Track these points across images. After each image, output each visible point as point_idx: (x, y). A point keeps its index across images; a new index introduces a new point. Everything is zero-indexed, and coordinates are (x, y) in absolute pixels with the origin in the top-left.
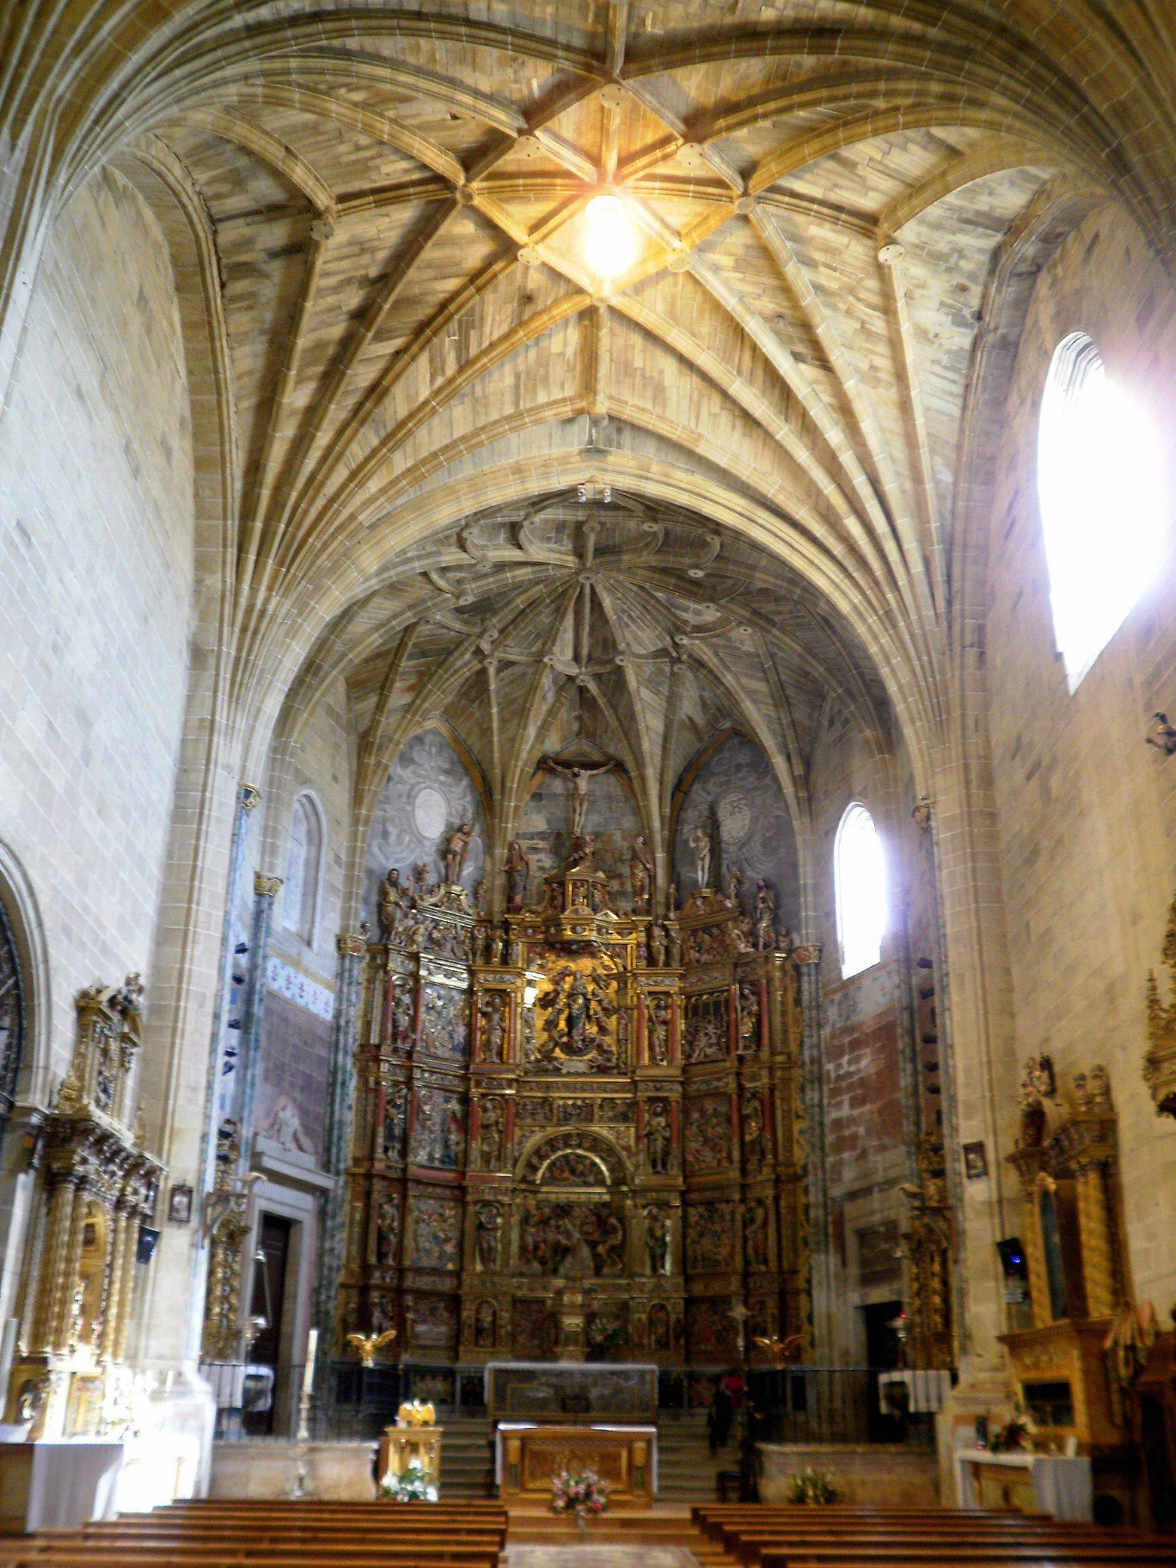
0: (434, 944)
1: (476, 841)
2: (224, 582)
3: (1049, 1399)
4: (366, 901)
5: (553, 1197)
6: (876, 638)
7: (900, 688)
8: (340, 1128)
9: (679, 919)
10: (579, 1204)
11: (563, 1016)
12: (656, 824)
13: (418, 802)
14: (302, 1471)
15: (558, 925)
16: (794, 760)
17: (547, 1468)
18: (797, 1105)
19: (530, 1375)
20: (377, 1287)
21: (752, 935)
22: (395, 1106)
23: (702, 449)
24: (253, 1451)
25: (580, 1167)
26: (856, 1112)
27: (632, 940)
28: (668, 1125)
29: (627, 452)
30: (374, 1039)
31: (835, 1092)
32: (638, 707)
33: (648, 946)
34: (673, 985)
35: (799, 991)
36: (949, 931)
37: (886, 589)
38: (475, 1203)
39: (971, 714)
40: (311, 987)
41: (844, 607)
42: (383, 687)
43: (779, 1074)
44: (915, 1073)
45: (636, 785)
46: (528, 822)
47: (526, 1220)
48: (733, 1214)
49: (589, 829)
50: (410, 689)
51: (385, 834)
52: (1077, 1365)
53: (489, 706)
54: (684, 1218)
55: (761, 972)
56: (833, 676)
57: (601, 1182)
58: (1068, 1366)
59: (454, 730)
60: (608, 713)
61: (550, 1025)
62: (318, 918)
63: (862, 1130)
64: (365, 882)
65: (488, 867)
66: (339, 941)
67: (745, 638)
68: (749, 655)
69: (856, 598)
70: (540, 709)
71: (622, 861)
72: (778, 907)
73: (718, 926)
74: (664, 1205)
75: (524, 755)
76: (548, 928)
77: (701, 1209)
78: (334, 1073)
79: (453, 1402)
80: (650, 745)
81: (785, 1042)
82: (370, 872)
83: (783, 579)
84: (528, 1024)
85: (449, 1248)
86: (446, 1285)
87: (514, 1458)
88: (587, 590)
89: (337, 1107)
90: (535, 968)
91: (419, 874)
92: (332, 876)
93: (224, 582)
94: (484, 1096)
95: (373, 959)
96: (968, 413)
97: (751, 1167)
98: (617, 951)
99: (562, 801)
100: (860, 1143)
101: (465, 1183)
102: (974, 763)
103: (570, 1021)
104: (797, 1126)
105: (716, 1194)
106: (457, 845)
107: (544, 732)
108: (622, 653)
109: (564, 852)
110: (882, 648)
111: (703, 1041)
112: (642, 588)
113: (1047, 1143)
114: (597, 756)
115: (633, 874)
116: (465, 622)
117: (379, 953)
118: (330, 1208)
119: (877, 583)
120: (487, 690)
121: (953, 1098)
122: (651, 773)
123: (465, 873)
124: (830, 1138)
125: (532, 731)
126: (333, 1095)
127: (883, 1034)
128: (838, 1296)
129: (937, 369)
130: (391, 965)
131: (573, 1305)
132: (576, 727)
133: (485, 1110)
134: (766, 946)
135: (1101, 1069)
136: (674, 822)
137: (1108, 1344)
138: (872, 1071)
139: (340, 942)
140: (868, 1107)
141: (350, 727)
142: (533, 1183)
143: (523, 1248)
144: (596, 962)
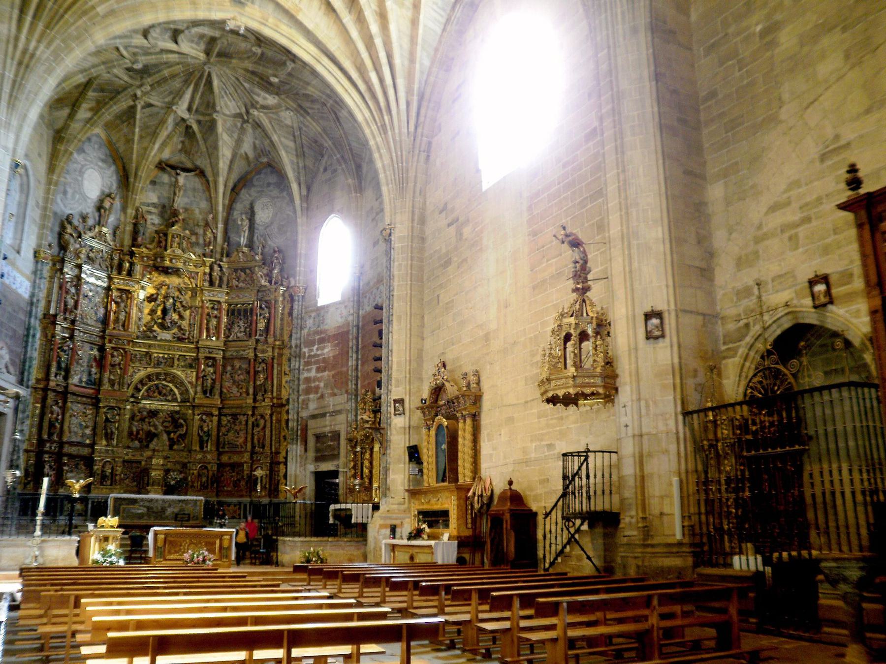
0: (90, 260)
1: (117, 203)
2: (10, 30)
3: (435, 518)
4: (52, 230)
5: (148, 406)
6: (374, 137)
7: (384, 166)
8: (31, 362)
9: (228, 262)
10: (162, 411)
11: (160, 308)
12: (220, 208)
13: (86, 176)
14: (37, 553)
15: (163, 258)
16: (302, 186)
17: (177, 549)
18: (286, 368)
19: (134, 501)
20: (47, 452)
21: (269, 276)
22: (63, 350)
23: (300, 17)
24: (4, 543)
25: (164, 391)
26: (319, 375)
27: (200, 270)
28: (215, 372)
29: (256, 7)
30: (52, 312)
31: (308, 363)
32: (220, 143)
33: (210, 275)
34: (223, 298)
35: (292, 309)
36: (395, 293)
37: (385, 113)
38: (104, 407)
39: (419, 186)
40: (20, 279)
41: (359, 117)
42: (74, 105)
43: (276, 351)
44: (357, 359)
45: (211, 184)
46: (148, 197)
47: (132, 418)
48: (247, 421)
49: (181, 205)
50: (91, 109)
51: (65, 193)
52: (455, 503)
53: (134, 125)
54: (219, 421)
55: (272, 297)
56: (336, 147)
57: (175, 400)
58: (449, 503)
59: (109, 136)
60: (201, 142)
61: (153, 312)
62: (25, 238)
63: (322, 384)
64: (52, 220)
65: (122, 219)
66: (35, 253)
67: (288, 117)
68: (287, 126)
69: (367, 114)
70: (164, 134)
71: (198, 225)
72: (284, 263)
73: (250, 269)
74: (211, 415)
75: (150, 159)
76: (156, 259)
77: (229, 418)
78: (28, 329)
79: (86, 515)
80: (223, 165)
81: (282, 335)
82: (55, 214)
83: (323, 93)
84: (140, 310)
85: (88, 432)
86: (85, 451)
87: (160, 544)
88: (206, 74)
89: (29, 349)
90: (146, 279)
91: (84, 218)
92: (33, 213)
93: (10, 30)
94: (113, 348)
95: (54, 265)
96: (445, 34)
97: (259, 398)
98: (193, 276)
99: (167, 188)
100: (320, 391)
101: (99, 396)
102: (417, 211)
103: (165, 312)
104: (285, 379)
105: (238, 411)
106: (107, 204)
107: (165, 148)
108: (217, 112)
109: (166, 216)
110: (377, 143)
111: (236, 329)
112: (238, 79)
113: (442, 403)
114: (189, 165)
115: (205, 234)
116: (131, 77)
117: (59, 263)
118: (21, 407)
119: (380, 109)
120: (134, 118)
121: (389, 376)
122: (221, 180)
123: (110, 220)
124: (302, 387)
125: (157, 146)
126: (27, 342)
127: (341, 337)
128: (301, 466)
129: (435, 7)
130: (65, 270)
131: (157, 464)
132: (180, 147)
133: (113, 356)
134: (276, 283)
135: (477, 372)
136: (230, 208)
137: (470, 494)
138: (331, 355)
139: (36, 254)
140: (326, 373)
141: (50, 125)
142: (137, 398)
143: (130, 433)
144: (180, 280)
